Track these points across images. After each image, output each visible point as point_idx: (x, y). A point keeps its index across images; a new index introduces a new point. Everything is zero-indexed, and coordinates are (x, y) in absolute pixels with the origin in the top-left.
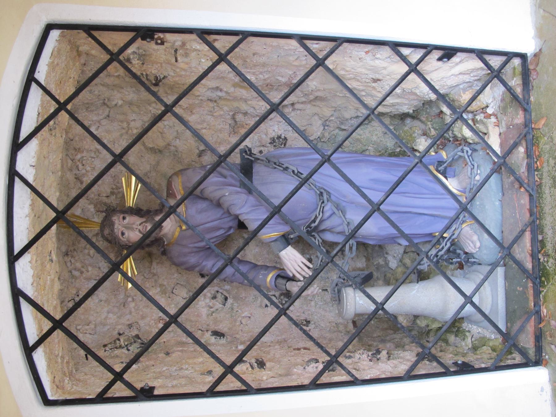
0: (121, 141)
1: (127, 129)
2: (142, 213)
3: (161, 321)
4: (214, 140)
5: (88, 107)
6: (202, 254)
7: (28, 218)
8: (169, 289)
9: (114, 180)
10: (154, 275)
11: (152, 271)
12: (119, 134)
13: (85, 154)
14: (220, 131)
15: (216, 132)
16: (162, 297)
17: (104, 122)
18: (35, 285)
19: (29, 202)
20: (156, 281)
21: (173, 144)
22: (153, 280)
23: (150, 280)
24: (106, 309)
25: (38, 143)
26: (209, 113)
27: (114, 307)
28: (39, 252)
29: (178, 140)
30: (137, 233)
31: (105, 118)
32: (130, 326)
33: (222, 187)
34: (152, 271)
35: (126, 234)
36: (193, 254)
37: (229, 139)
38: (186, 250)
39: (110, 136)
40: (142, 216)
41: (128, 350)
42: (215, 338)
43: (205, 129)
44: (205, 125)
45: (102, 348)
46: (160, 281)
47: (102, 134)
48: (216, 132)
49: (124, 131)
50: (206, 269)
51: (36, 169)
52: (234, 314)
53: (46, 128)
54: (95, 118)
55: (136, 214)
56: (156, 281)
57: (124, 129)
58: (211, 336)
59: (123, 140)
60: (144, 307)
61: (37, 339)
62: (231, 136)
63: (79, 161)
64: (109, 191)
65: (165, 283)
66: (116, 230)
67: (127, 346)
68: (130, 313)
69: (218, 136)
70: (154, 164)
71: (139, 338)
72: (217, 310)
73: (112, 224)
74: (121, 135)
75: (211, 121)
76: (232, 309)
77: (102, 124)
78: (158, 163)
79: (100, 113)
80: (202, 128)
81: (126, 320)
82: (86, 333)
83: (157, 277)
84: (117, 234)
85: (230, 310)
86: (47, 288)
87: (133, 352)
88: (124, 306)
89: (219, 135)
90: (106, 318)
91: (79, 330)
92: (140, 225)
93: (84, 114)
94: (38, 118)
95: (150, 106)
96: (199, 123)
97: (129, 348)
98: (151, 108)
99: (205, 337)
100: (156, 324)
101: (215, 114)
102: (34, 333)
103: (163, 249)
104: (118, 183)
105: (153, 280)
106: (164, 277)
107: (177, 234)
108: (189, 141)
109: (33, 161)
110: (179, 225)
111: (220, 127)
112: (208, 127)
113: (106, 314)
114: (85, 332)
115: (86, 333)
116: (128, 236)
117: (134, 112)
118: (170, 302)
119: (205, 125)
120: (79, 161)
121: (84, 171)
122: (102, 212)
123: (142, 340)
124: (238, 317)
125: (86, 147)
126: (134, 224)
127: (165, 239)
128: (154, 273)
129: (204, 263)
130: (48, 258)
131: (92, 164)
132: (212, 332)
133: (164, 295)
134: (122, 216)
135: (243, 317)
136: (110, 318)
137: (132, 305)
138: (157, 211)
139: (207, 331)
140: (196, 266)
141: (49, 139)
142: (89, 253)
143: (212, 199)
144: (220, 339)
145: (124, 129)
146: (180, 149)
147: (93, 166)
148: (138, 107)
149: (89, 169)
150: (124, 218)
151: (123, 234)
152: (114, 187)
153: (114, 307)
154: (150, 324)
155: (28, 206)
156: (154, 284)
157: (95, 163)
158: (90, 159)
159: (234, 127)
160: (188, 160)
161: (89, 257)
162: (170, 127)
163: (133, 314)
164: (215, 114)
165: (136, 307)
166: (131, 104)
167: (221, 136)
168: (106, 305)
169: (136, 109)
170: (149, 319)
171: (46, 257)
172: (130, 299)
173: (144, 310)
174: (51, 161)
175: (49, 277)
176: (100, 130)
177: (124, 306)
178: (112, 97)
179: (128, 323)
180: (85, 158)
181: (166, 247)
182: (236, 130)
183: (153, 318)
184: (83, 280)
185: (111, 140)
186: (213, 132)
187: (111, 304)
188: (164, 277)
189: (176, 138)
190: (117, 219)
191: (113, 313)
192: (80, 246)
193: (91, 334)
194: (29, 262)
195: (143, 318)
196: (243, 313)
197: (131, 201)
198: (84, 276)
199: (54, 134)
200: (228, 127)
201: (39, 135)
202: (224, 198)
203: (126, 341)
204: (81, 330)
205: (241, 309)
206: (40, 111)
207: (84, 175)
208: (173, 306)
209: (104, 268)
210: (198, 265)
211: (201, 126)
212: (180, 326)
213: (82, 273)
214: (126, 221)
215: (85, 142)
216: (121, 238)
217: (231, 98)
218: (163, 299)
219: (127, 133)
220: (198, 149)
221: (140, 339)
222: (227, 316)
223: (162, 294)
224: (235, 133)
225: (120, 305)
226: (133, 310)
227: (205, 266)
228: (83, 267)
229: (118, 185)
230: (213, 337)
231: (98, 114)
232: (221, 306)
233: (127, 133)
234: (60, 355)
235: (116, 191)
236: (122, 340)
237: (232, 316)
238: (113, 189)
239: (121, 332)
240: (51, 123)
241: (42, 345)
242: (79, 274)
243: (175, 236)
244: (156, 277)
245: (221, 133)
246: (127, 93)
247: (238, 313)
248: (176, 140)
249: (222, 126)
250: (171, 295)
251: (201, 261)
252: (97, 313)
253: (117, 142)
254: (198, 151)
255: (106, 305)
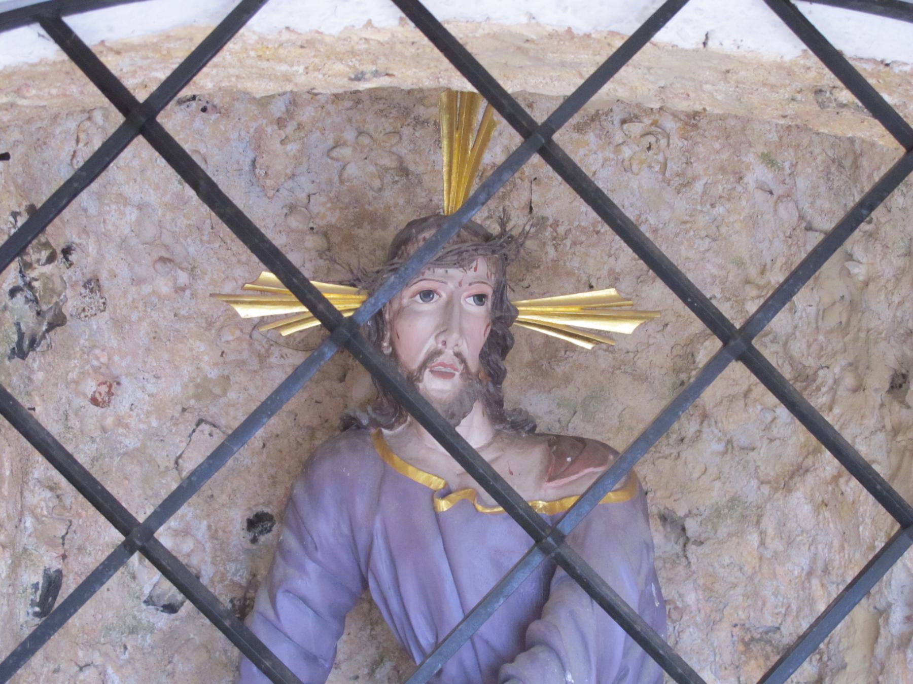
0: (719, 261)
1: (762, 282)
2: (495, 357)
3: (104, 389)
4: (722, 572)
5: (840, 165)
6: (345, 558)
7: (524, 20)
8: (213, 410)
9: (583, 230)
10: (262, 358)
11: (276, 351)
12: (746, 256)
13: (676, 142)
14: (754, 595)
15: (751, 578)
16: (185, 387)
17: (787, 212)
18: (286, 36)
19: (581, 26)
20: (241, 364)
21: (706, 429)
22: (245, 355)
23: (245, 345)
24: (153, 198)
25: (787, 58)
26: (820, 565)
27: (160, 224)
28: (399, 47)
29: (720, 447)
30: (430, 344)
31: (801, 217)
32: (93, 284)
33: (593, 659)
34: (276, 351)
35: (426, 307)
36: (345, 530)
37: (725, 626)
38: (361, 506)
39: (737, 226)
40: (483, 355)
41: (13, 292)
42: (36, 586)
43: (762, 543)
44: (775, 545)
45: (25, 203)
46: (239, 378)
47: (744, 203)
48: (751, 578)
49: (753, 272)
50: (291, 571)
51: (696, 51)
52: (114, 635)
53: (829, 78)
54: (802, 183)
55: (493, 334)
56: (241, 364)
57: (763, 272)
58: (46, 571)
59: (721, 267)
60: (155, 325)
61: (90, 40)
62: (736, 631)
63: (655, 123)
64: (549, 212)
65: (232, 395)
66: (440, 271)
67: (29, 286)
68: (137, 281)
69: (734, 586)
70: (639, 363)
71: (51, 327)
72: (134, 577)
73: (461, 260)
74: (740, 263)
75: (789, 566)
76: (133, 631)
77: (782, 207)
78: (641, 378)
79: (819, 202)
80: (763, 534)
81: (114, 268)
82: (78, 141)
83: (256, 367)
84: (428, 274)
85: (129, 621)
86: (265, 64)
87: (5, 308)
88: (163, 260)
89: (740, 590)
90: (123, 200)
91: (89, 119)
92: (458, 355)
93: (817, 151)
94: (868, 60)
95: (843, 369)
96: (781, 524)
97: (20, 297)
98: (837, 370)
99: (43, 549)
100: (96, 370)
101: (815, 582)
102: (111, 29)
103: (365, 422)
104: (574, 243)
105: (245, 355)
106: (252, 391)
107: (421, 477)
108: (718, 484)
109: (723, 43)
110: (453, 486)
111: (768, 593)
112: (768, 554)
113: (136, 198)
114: (83, 136)
115: (78, 141)
116: (419, 313)
117: (822, 313)
118: (169, 412)
119: (775, 545)
120: (655, 123)
121: (619, 138)
122: (503, 224)
123: (44, 337)
124: (105, 655)
125: (701, 149)
126: (461, 332)
127: (400, 429)
128: (268, 354)
129: (311, 567)
130: (369, 68)
131: (642, 163)
132: (59, 572)
133: (191, 391)
134: (488, 290)
135: (103, 674)
136: (122, 214)
137: (164, 286)
138: (500, 403)
139: (64, 557)
140: (301, 539)
141: (785, 86)
142: (345, 144)
143: (548, 618)
144: (33, 603)
145: (763, 272)
146: (688, 453)
147: (635, 168)
148: (843, 328)
149: (627, 152)
150: (480, 298)
151: (427, 295)
152: (561, 230)
153: (160, 224)
154: (97, 351)
155: (570, 24)
156: (231, 357)
157: (645, 173)
158: (660, 158)
159: (769, 642)
160: (650, 477)
161: (331, 143)
162: (768, 428)
163: (133, 289)
164: (815, 582)
165: (154, 299)
166: (854, 306)
167: (737, 596)
168: (167, 198)
169: (833, 320)
170: (114, 343)
171: (374, 62)
172: (183, 278)
173: (145, 326)
174: (708, 87)
175: (301, 69)
176: (760, 196)
177: (163, 260)
178: (879, 247)
179: (104, 276)
180: (663, 142)
181: (373, 431)
182: (756, 648)
183: (116, 358)
184: (254, 125)
185: (723, 230)
186: (748, 570)
187: (169, 216)
188: (252, 391)
189: (729, 441)
190: (480, 272)
191: (139, 222)
192: (370, 117)
193: (74, 156)
194: (369, 23)
195: (118, 324)
196: (119, 668)
197: (534, 314)
198: (269, 129)
199: (799, 97)
200: (769, 620)
201: (813, 60)
202: (554, 667)
203: (45, 285)
204: (87, 124)
205: (130, 661)
206: (896, 69)
207: (607, 136)
208: (155, 424)
209: (291, 190)
210: (305, 548)
211: (771, 532)
212: (114, 561)
213: (281, 123)
214: (470, 305)
215: (717, 146)
216: (414, 288)
217: (880, 650)
218: (178, 388)
219: (747, 282)
220: (689, 514)
221: (48, 331)
222: (110, 614)
223: (198, 386)
224: (747, 645)
225: (167, 248)
226: (146, 289)
227: (301, 568)
228: (300, 127)
229: (568, 242)
230: (38, 578)
231: (815, 196)
232: (147, 590)
233: (747, 282)
234: (21, 102)
235: (548, 233)
236: (48, 269)
237: (108, 629)
238: (556, 224)
239: (73, 257)
240: (846, 95)
241: (64, 56)
242: (278, 115)
243: (411, 468)
244: (254, 364)
245: (746, 596)
246: (896, 299)
247: (119, 650)
248: (720, 440)
249: (771, 601)
250: (191, 418)
251: (319, 555)
252: (143, 171)
253: (714, 244)
254: (681, 513)
255: (167, 198)
